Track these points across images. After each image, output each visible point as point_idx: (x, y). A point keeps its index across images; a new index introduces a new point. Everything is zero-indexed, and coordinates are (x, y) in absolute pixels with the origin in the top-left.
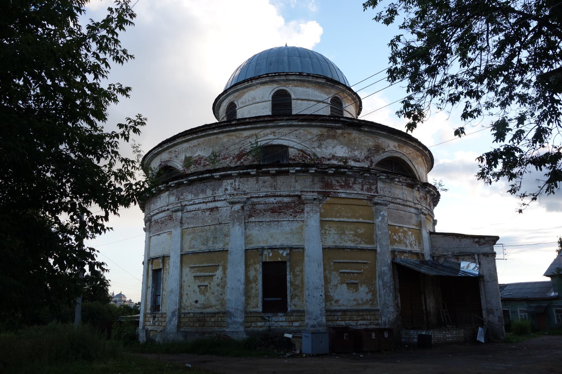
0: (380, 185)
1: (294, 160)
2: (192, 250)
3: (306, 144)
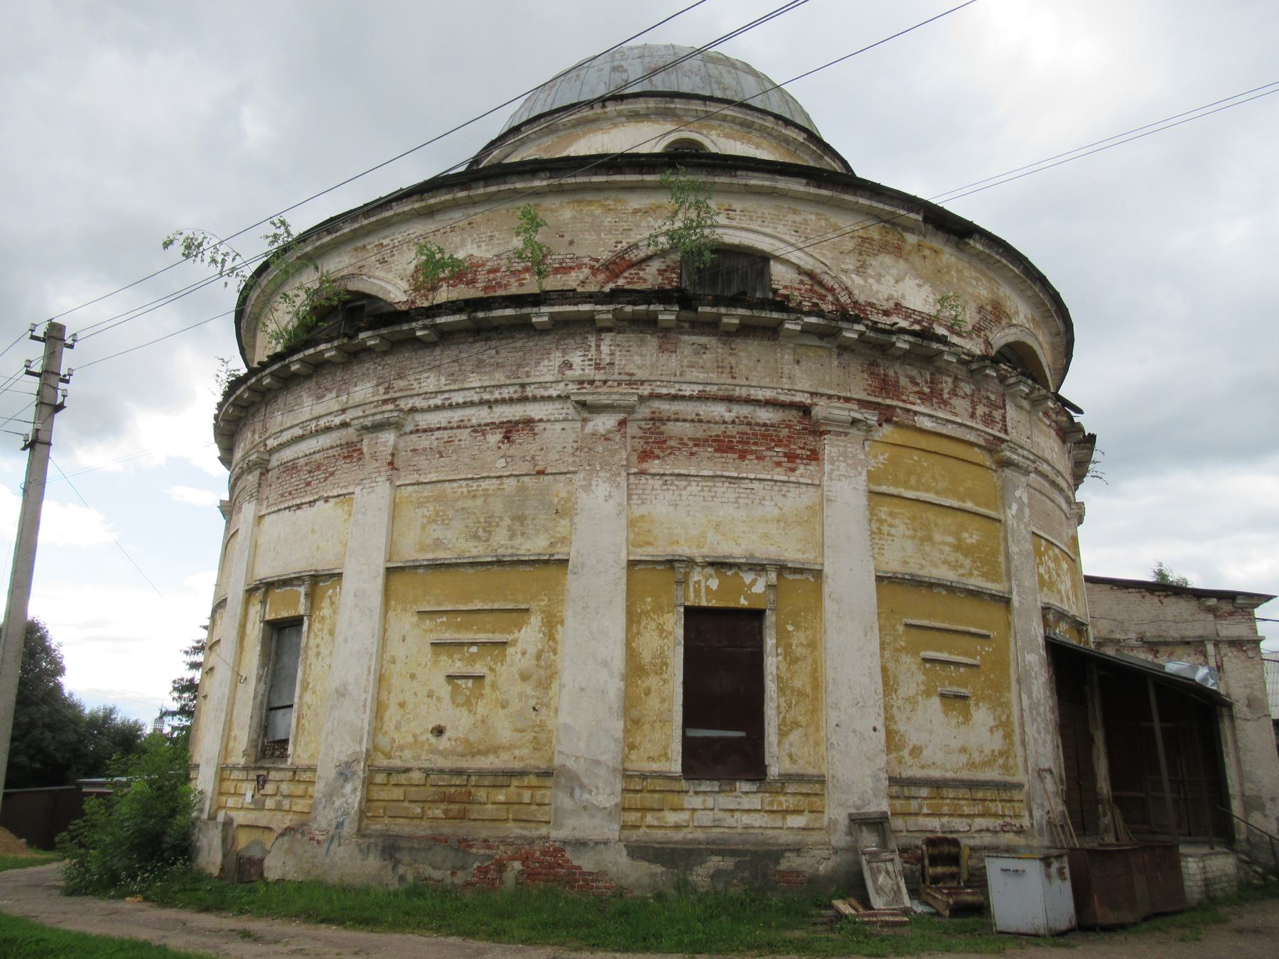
2: (431, 556)
3: (824, 255)
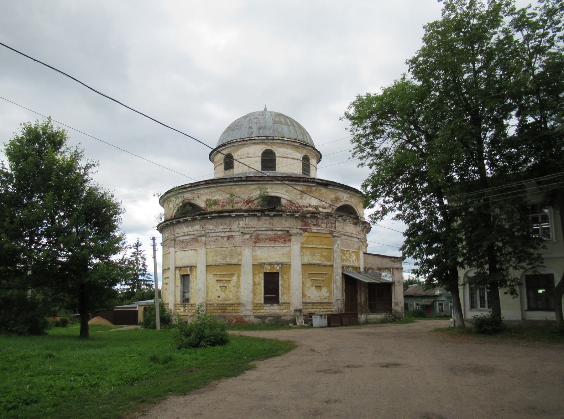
0: (337, 224)
1: (285, 206)
